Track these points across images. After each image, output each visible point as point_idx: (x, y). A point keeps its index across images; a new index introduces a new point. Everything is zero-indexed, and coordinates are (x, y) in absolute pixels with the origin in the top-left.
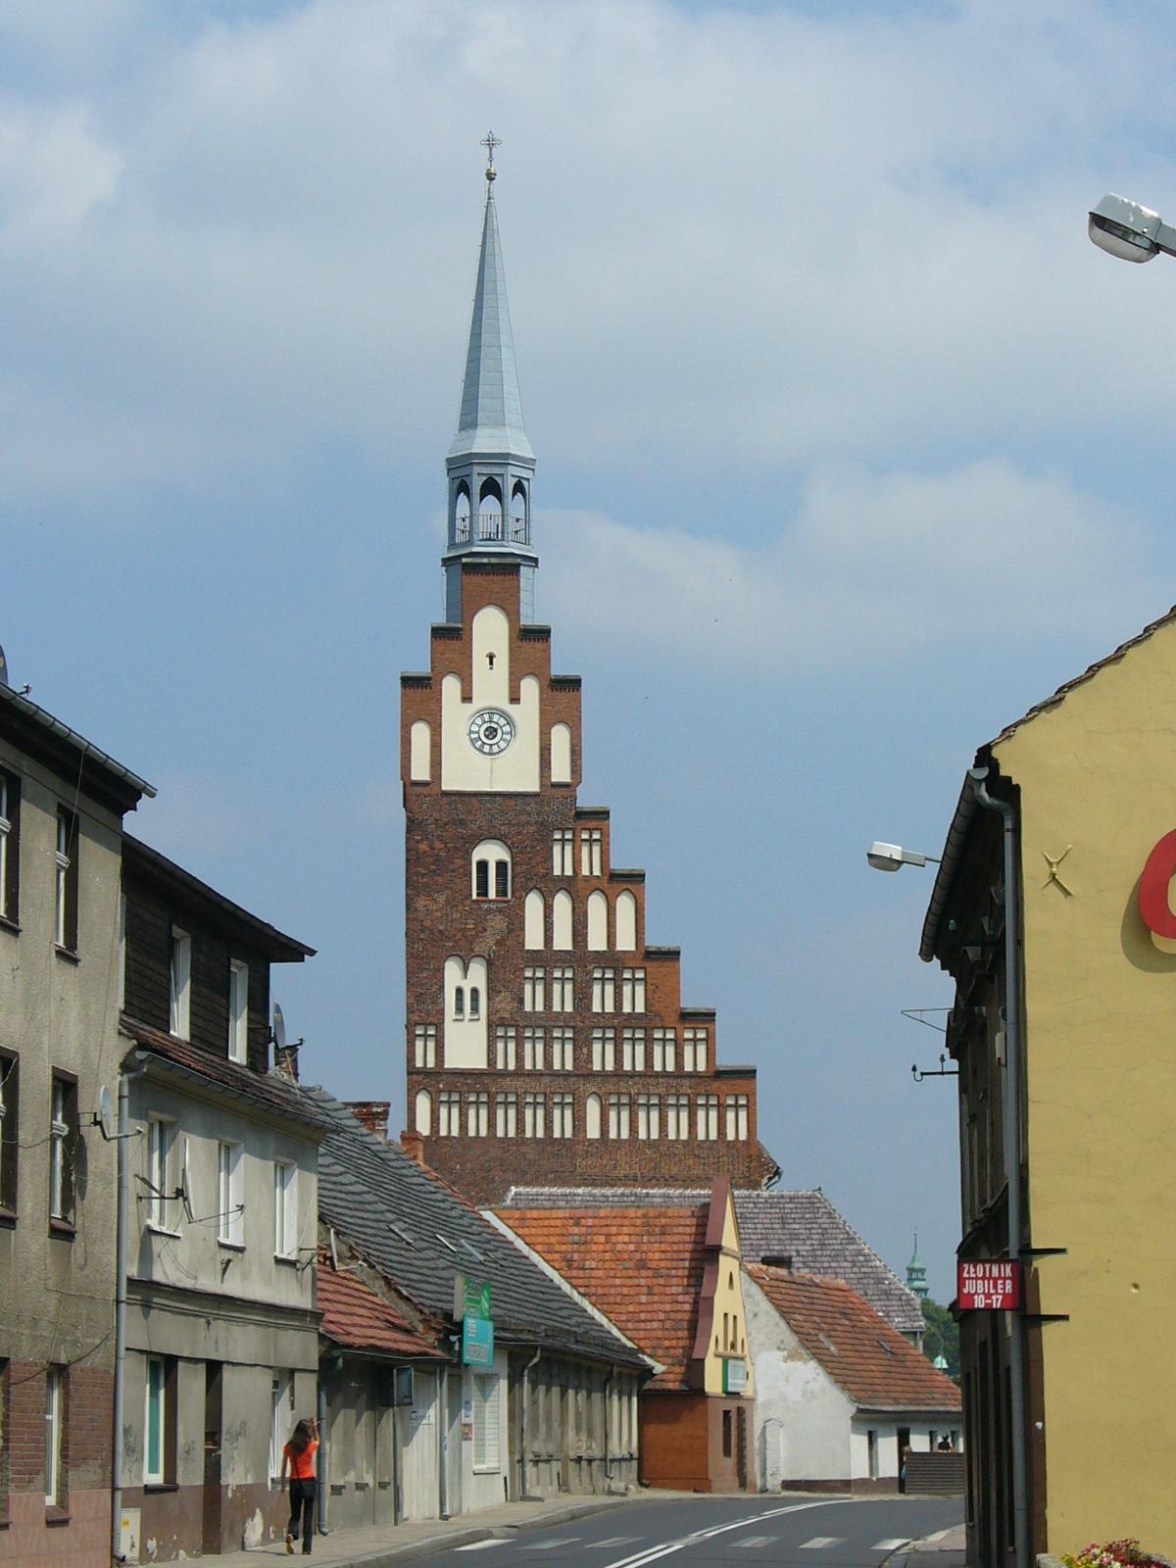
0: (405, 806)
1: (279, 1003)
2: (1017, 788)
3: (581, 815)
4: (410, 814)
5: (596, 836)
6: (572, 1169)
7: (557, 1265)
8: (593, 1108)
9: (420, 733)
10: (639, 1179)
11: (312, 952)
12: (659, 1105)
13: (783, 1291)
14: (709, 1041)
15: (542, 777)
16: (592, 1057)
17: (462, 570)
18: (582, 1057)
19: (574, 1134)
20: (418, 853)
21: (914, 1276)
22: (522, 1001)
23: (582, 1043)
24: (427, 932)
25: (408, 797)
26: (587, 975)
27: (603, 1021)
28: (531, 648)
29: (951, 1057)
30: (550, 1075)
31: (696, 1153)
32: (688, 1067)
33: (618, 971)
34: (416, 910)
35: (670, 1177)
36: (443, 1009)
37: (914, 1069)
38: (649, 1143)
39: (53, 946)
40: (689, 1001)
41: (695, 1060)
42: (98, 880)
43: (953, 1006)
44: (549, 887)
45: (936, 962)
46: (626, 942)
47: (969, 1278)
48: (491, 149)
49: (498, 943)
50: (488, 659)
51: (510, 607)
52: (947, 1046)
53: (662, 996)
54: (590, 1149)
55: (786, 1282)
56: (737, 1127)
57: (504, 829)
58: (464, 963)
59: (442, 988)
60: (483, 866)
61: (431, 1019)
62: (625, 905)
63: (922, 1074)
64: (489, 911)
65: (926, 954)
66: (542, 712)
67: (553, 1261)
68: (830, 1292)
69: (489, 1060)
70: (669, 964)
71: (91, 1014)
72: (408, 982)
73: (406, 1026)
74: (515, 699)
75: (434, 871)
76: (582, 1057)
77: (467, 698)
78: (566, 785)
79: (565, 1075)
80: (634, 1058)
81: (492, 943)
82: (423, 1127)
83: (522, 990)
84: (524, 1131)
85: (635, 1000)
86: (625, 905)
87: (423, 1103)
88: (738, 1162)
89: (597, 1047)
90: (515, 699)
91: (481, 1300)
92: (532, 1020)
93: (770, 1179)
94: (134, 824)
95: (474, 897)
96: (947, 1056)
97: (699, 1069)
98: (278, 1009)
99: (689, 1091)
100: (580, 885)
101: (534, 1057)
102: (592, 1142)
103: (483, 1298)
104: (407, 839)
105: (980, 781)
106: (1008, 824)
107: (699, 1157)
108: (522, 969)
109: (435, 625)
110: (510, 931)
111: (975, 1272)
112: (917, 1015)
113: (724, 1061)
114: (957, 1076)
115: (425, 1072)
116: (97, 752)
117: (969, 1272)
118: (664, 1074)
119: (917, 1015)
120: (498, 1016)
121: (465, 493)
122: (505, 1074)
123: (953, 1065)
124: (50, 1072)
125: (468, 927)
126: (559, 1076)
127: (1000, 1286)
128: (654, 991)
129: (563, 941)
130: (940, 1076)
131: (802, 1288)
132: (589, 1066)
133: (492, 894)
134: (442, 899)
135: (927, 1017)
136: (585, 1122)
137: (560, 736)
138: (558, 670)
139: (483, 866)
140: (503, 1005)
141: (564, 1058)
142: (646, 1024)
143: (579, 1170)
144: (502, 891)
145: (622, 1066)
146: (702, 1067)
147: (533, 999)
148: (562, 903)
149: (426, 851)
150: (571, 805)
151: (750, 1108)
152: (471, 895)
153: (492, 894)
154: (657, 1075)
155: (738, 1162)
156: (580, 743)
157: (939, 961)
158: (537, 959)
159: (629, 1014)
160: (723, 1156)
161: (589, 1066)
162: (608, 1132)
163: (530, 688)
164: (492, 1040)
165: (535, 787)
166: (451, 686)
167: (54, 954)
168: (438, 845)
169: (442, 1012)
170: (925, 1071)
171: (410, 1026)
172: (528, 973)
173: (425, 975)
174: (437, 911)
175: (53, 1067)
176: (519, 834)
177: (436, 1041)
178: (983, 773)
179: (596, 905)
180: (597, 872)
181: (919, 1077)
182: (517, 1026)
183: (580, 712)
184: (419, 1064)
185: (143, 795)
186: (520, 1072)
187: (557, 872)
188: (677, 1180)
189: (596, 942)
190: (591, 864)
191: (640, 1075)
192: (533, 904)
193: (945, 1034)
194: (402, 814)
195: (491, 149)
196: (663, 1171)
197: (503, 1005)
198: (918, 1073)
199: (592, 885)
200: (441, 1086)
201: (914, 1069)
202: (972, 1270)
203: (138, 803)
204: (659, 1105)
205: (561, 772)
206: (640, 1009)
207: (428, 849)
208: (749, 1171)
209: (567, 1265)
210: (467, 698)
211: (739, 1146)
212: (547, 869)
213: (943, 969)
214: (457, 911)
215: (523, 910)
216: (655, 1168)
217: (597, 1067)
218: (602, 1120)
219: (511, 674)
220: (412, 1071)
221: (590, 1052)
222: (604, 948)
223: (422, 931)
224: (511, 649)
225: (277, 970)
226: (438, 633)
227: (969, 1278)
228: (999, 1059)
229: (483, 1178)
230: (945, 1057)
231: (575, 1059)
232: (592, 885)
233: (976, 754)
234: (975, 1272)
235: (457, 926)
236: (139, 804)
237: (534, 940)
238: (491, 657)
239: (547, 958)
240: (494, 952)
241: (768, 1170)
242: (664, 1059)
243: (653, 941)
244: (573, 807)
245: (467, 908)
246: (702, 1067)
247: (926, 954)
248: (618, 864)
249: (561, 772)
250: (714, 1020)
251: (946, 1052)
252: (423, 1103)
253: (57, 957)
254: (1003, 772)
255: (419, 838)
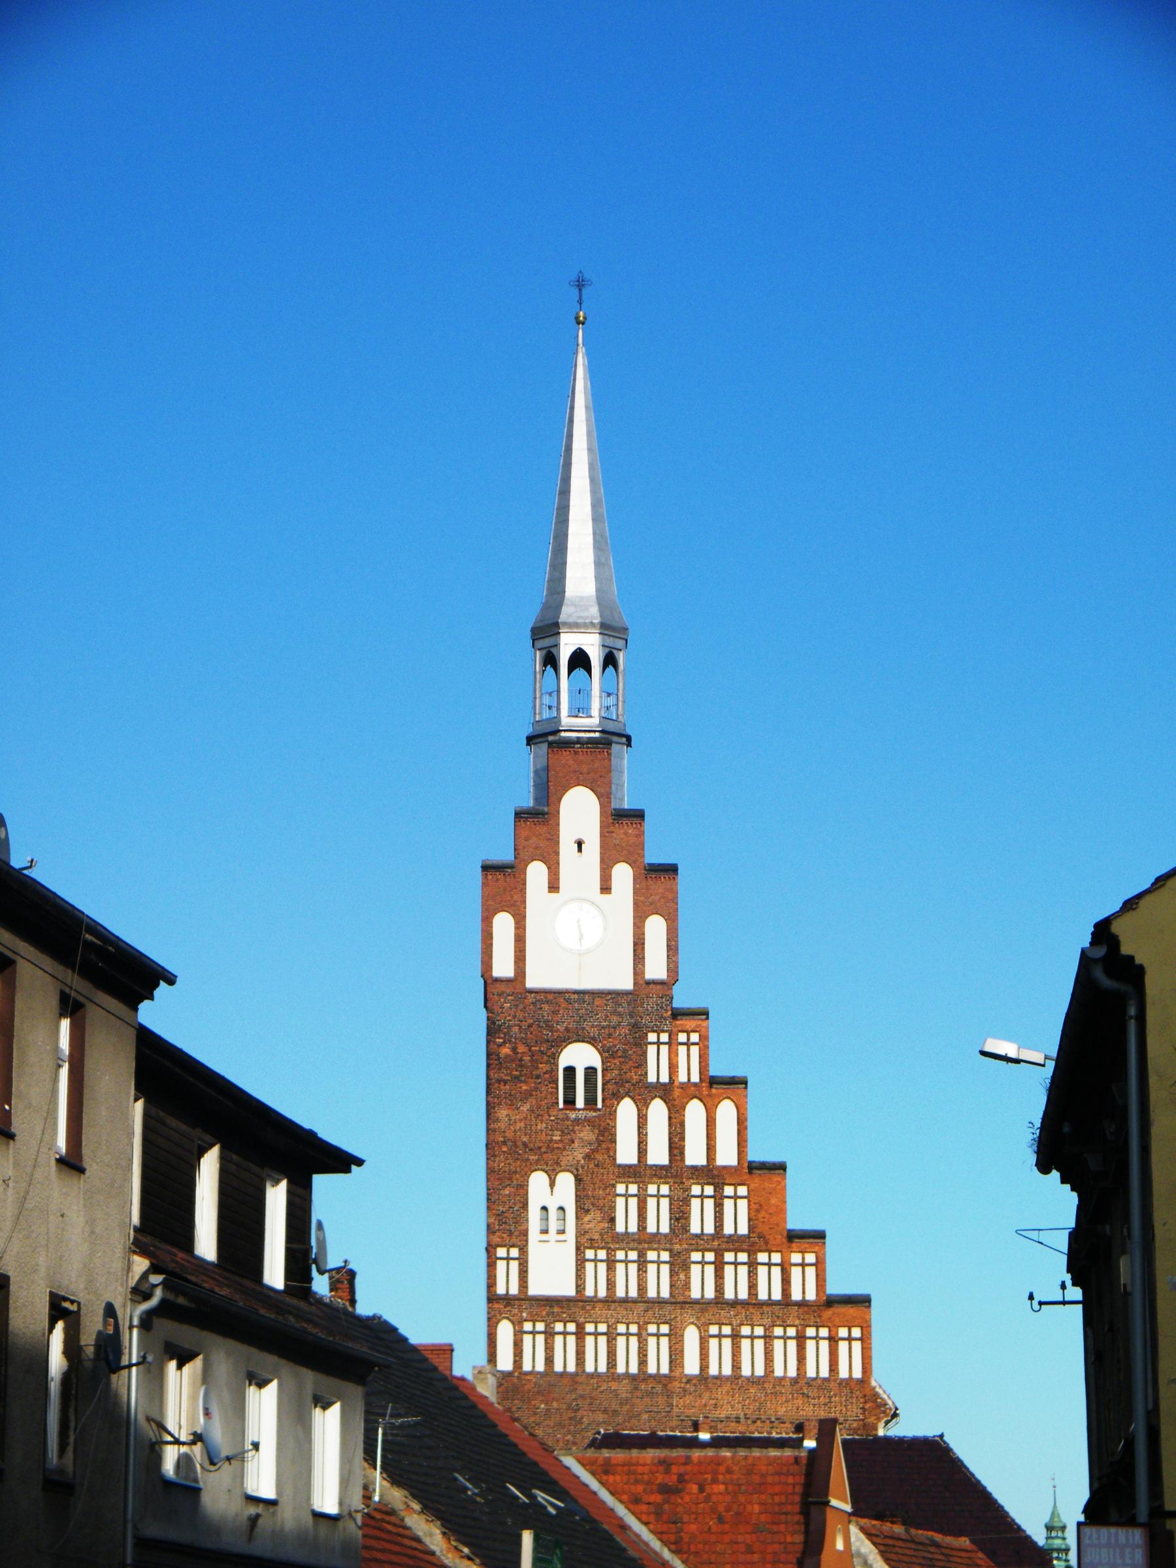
0: (486, 1006)
1: (320, 1218)
2: (1141, 970)
3: (677, 1014)
4: (490, 1015)
5: (695, 1037)
6: (668, 1409)
7: (644, 1517)
8: (691, 1336)
9: (503, 923)
10: (742, 1420)
11: (360, 1162)
12: (764, 1337)
13: (899, 1551)
14: (819, 1265)
15: (635, 974)
16: (689, 1283)
17: (549, 748)
18: (679, 1281)
19: (671, 1370)
20: (499, 1058)
21: (1054, 1534)
22: (612, 1220)
23: (679, 1266)
24: (510, 1144)
25: (490, 996)
26: (684, 1191)
27: (700, 1242)
28: (627, 830)
29: (1074, 1284)
30: (645, 1302)
31: (806, 1391)
32: (796, 1295)
33: (718, 1188)
34: (498, 1120)
35: (777, 1419)
36: (527, 1230)
37: (1031, 1297)
38: (753, 1381)
39: (52, 1153)
40: (796, 1220)
41: (804, 1287)
42: (107, 1078)
43: (1073, 1225)
44: (643, 1093)
45: (1055, 1175)
46: (727, 1156)
47: (1091, 1546)
48: (580, 290)
49: (587, 1157)
50: (576, 845)
51: (602, 788)
52: (1068, 1272)
53: (767, 1216)
54: (688, 1386)
55: (902, 1540)
56: (850, 1365)
57: (594, 1032)
58: (550, 1178)
59: (525, 1205)
60: (570, 1071)
61: (514, 1240)
62: (726, 1111)
63: (1041, 1303)
64: (577, 1121)
65: (1044, 1166)
66: (636, 904)
67: (642, 1513)
68: (951, 1553)
69: (577, 1286)
70: (776, 1179)
71: (97, 1230)
72: (488, 1199)
73: (486, 1249)
74: (606, 888)
75: (516, 1077)
76: (679, 1281)
77: (554, 887)
78: (661, 983)
79: (659, 1302)
80: (736, 1285)
81: (580, 1157)
82: (505, 1362)
83: (613, 1208)
84: (615, 1365)
85: (737, 1219)
86: (726, 1111)
87: (505, 1330)
88: (852, 1403)
89: (695, 1270)
90: (606, 888)
91: (553, 1559)
92: (625, 1240)
93: (887, 1423)
94: (150, 1014)
95: (561, 1105)
96: (1069, 1283)
97: (807, 1298)
98: (320, 1226)
99: (797, 1322)
100: (677, 1093)
101: (626, 1284)
102: (689, 1379)
103: (555, 1558)
104: (488, 1042)
105: (1096, 961)
106: (1132, 1011)
107: (808, 1397)
108: (614, 1186)
109: (518, 809)
110: (599, 1142)
111: (1098, 1538)
112: (1034, 1235)
113: (834, 1288)
114: (1080, 1307)
115: (507, 1299)
116: (103, 930)
117: (1090, 1538)
118: (770, 1303)
119: (1034, 1235)
120: (587, 1237)
121: (552, 666)
122: (594, 1300)
123: (1076, 1293)
124: (46, 1299)
125: (554, 1138)
126: (654, 1302)
127: (1127, 1556)
128: (758, 1211)
129: (658, 1155)
130: (1061, 1306)
131: (920, 1547)
132: (686, 1293)
133: (580, 1102)
134: (525, 1108)
135: (1044, 1237)
136: (682, 1357)
137: (656, 927)
138: (654, 855)
139: (570, 1071)
140: (591, 1225)
141: (659, 1283)
142: (752, 1243)
143: (675, 1410)
144: (590, 1100)
145: (723, 1294)
146: (811, 1295)
147: (626, 1219)
148: (658, 1111)
149: (509, 1055)
150: (667, 1005)
151: (865, 1340)
152: (557, 1103)
153: (580, 1102)
154: (762, 1304)
155: (852, 1403)
156: (677, 937)
157: (1059, 1174)
158: (632, 1173)
159: (731, 1236)
160: (835, 1395)
161: (686, 1293)
162: (708, 1367)
163: (623, 874)
164: (581, 1262)
165: (627, 984)
166: (536, 873)
167: (53, 1163)
168: (521, 1049)
169: (525, 1233)
170: (1043, 1300)
171: (490, 1249)
172: (620, 1189)
173: (507, 1192)
174: (521, 1120)
175: (51, 1293)
176: (610, 1035)
177: (782, 1270)
178: (1100, 952)
179: (695, 1112)
180: (695, 1078)
181: (1036, 1307)
182: (608, 1249)
183: (677, 904)
184: (501, 1290)
185: (162, 983)
186: (611, 1300)
187: (652, 1078)
188: (784, 1423)
189: (695, 1155)
190: (689, 1070)
191: (743, 1303)
192: (626, 1110)
193: (1065, 1258)
194: (483, 1014)
195: (580, 290)
196: (768, 1413)
197: (591, 1225)
198: (1035, 1303)
199: (690, 1091)
200: (524, 1315)
201: (1031, 1297)
202: (1095, 1536)
203: (155, 992)
204: (764, 1337)
205: (656, 969)
206: (743, 1229)
207: (510, 1053)
208: (863, 1413)
209: (658, 1519)
210: (554, 887)
211: (852, 1384)
212: (641, 1075)
213: (1063, 1182)
214: (542, 1121)
215: (614, 1119)
216: (759, 1410)
217: (695, 1294)
218: (701, 1354)
219: (602, 861)
220: (492, 1298)
221: (688, 1277)
222: (703, 1162)
223: (504, 1143)
224: (602, 836)
225: (320, 1182)
226: (520, 815)
227: (1091, 1546)
228: (1125, 1286)
229: (571, 1418)
230: (1067, 1284)
231: (671, 1286)
232: (690, 1091)
233: (1138, 961)
234: (1098, 1538)
235: (543, 1137)
236: (157, 993)
237: (626, 1154)
238: (580, 844)
239: (640, 1172)
240: (583, 1167)
241: (884, 1412)
242: (769, 1287)
243: (754, 1155)
244: (669, 1008)
245: (552, 1118)
246: (811, 1295)
247: (1044, 1166)
248: (717, 1069)
249: (656, 969)
250: (824, 1243)
251: (1068, 1278)
252: (505, 1330)
253: (59, 1171)
254: (1125, 950)
255: (501, 1040)
